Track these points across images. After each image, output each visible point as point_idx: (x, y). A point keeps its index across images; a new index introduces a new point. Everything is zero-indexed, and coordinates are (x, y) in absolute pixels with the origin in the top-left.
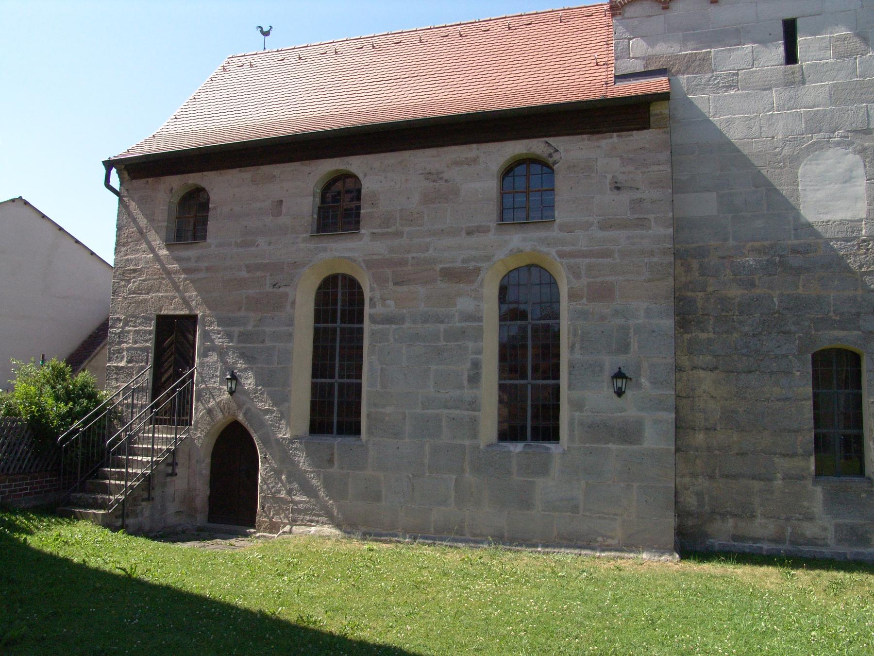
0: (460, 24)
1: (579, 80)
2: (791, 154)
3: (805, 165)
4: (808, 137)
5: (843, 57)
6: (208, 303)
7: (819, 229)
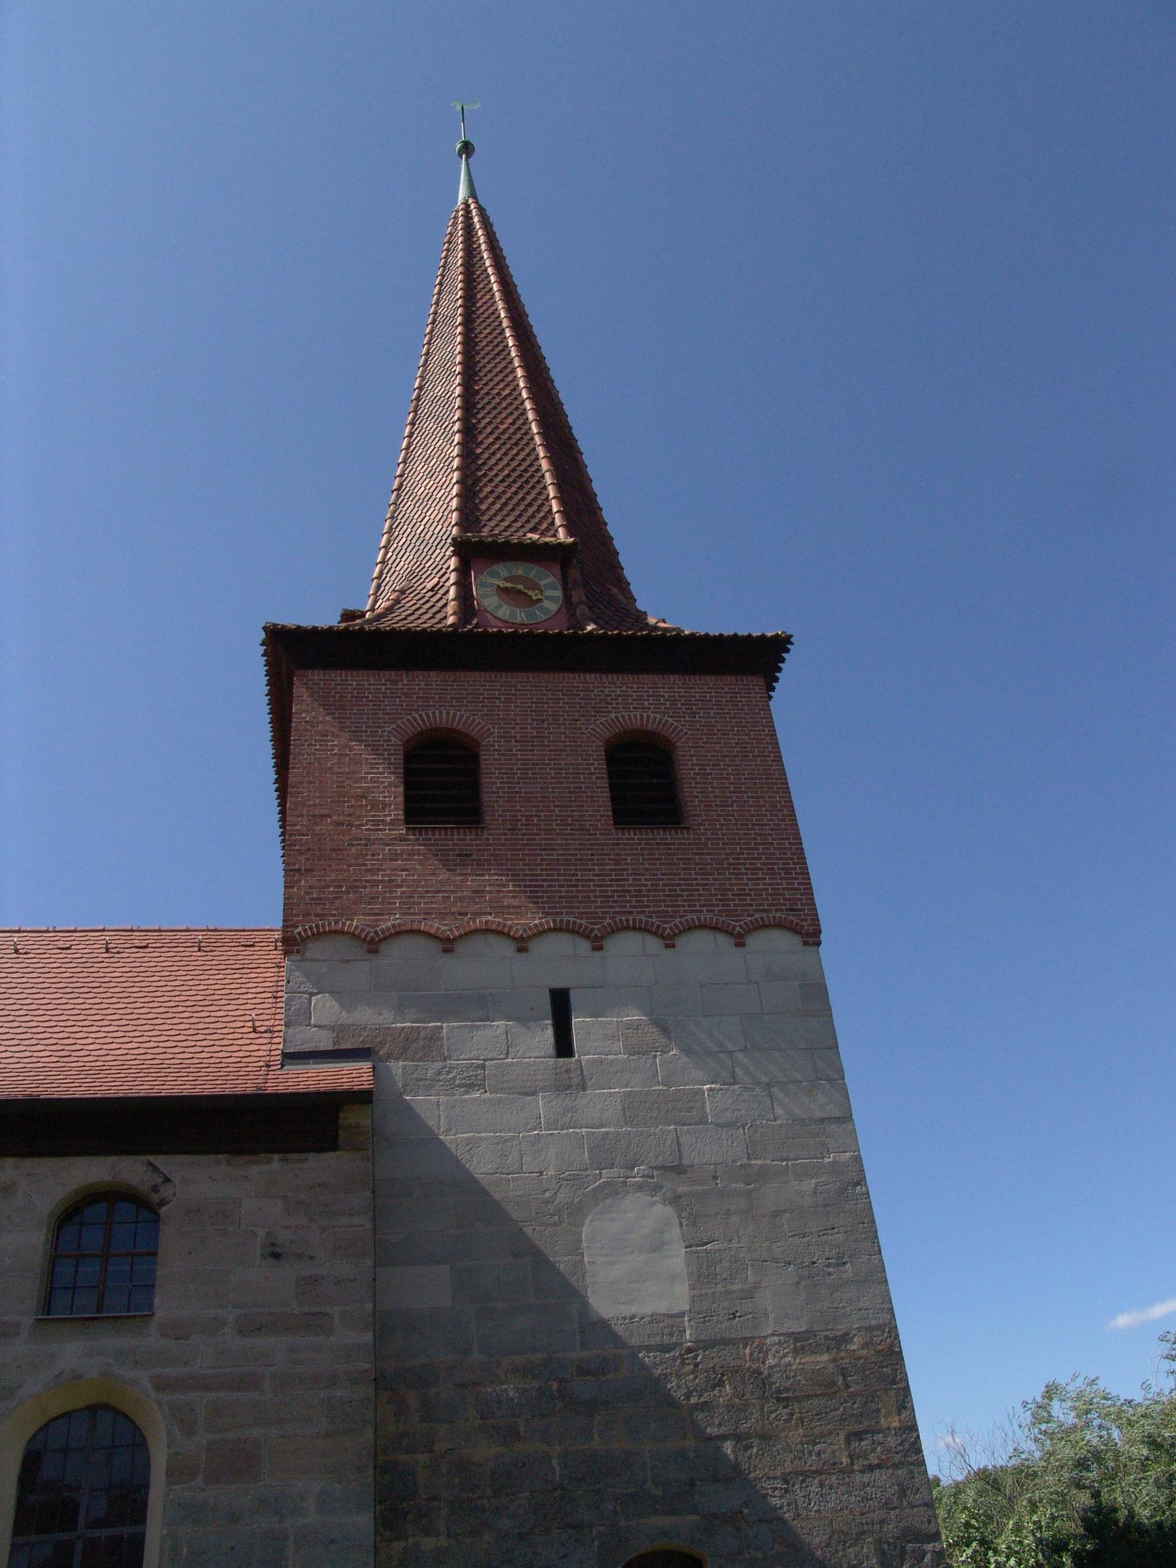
0: (19, 931)
1: (220, 1055)
2: (570, 1201)
3: (592, 1220)
4: (595, 1174)
5: (639, 1053)
7: (620, 1330)
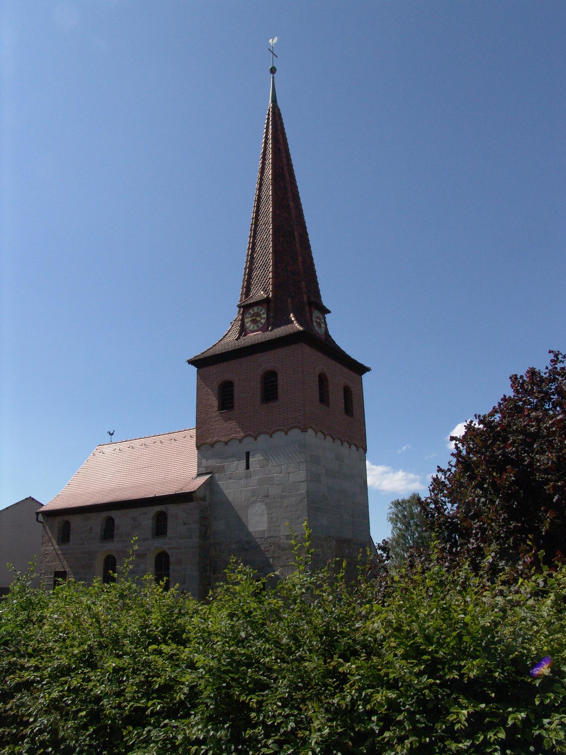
6: (70, 567)
